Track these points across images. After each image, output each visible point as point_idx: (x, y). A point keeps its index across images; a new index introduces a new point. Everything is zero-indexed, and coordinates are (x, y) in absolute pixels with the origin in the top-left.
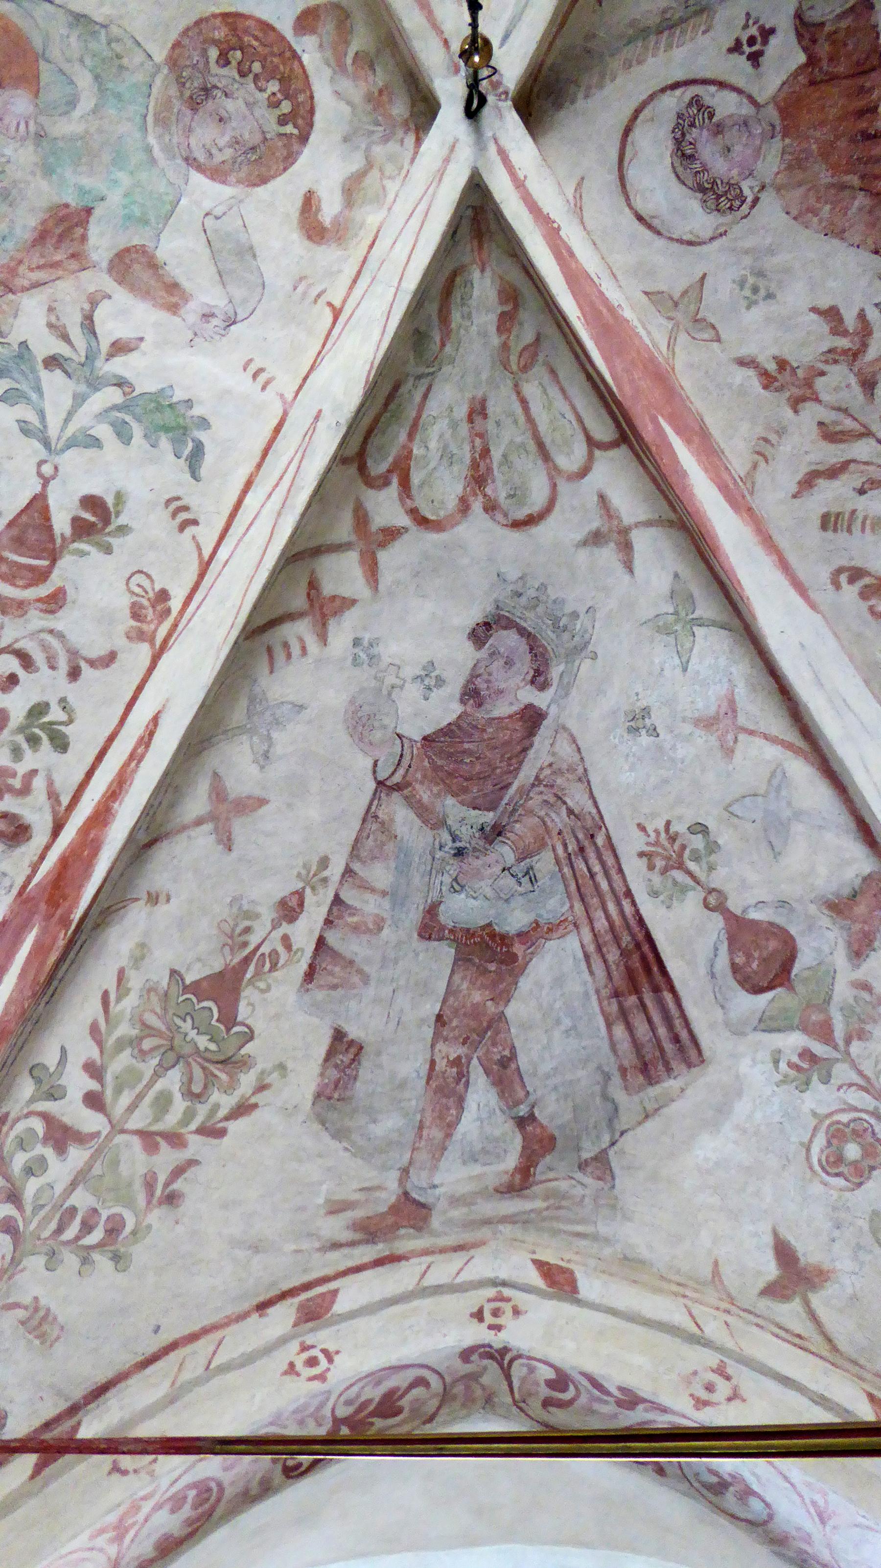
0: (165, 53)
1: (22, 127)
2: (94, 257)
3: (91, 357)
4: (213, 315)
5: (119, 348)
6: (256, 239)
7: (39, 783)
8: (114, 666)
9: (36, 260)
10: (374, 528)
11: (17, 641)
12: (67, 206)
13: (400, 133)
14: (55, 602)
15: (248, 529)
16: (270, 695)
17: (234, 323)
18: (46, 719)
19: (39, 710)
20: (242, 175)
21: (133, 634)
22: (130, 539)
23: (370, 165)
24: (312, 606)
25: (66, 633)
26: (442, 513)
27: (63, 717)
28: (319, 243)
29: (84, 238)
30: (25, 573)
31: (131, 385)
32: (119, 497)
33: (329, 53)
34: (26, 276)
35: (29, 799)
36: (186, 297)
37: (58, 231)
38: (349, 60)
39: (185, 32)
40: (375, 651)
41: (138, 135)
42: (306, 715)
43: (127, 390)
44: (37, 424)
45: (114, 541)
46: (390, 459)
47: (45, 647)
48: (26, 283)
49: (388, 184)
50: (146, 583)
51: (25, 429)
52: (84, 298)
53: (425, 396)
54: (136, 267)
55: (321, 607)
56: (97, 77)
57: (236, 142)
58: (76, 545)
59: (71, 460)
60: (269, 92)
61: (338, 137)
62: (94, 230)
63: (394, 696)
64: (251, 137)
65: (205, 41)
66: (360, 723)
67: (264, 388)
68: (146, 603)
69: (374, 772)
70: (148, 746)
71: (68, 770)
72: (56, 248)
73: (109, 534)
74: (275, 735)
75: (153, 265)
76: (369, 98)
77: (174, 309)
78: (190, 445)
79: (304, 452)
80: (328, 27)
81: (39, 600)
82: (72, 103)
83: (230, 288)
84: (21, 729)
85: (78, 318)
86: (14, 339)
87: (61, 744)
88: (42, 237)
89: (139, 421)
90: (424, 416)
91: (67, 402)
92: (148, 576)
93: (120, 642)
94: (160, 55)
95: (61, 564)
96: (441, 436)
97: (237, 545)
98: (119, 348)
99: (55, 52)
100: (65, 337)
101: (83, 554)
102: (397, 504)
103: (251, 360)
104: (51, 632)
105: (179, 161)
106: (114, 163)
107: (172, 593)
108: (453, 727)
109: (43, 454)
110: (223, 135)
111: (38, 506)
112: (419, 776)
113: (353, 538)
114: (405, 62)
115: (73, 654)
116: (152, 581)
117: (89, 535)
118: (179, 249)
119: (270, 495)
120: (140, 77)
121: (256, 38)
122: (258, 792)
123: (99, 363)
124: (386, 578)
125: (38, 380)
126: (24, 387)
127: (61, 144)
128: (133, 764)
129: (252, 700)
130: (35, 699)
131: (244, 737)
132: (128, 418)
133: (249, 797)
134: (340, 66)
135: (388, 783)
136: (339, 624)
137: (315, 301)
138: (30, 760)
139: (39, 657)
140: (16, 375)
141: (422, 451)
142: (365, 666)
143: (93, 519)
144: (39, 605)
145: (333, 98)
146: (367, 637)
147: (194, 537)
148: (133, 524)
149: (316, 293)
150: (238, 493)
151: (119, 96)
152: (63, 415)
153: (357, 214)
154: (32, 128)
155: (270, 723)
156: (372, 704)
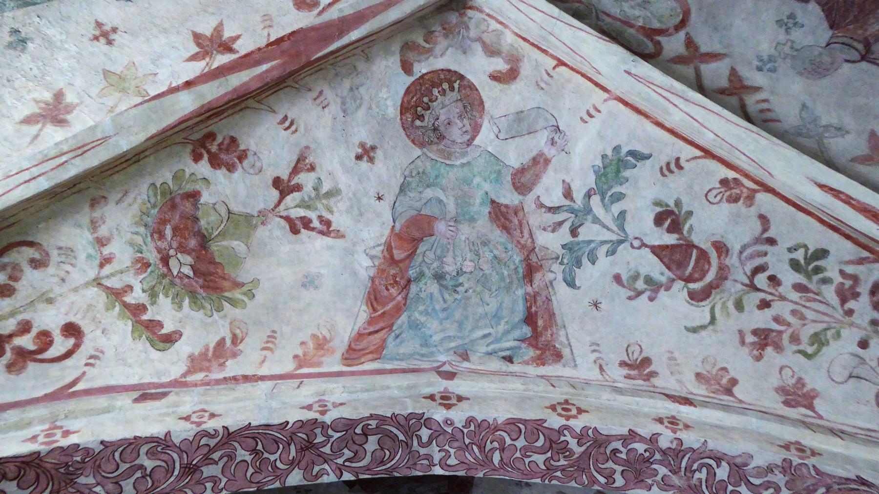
0: (417, 149)
1: (451, 228)
2: (516, 202)
3: (572, 211)
4: (553, 139)
5: (568, 194)
6: (513, 110)
7: (850, 269)
8: (769, 216)
9: (517, 233)
10: (686, 53)
11: (745, 273)
12: (490, 213)
13: (466, 19)
14: (721, 248)
15: (696, 120)
16: (795, 124)
17: (558, 127)
18: (802, 262)
19: (795, 265)
20: (478, 115)
21: (748, 203)
22: (685, 200)
23: (480, 39)
24: (735, 94)
25: (742, 244)
26: (679, 10)
27: (802, 250)
28: (518, 73)
29: (507, 206)
30: (700, 265)
31: (590, 190)
32: (657, 203)
33: (423, 57)
34: (526, 239)
35: (861, 277)
36: (541, 154)
37: (503, 219)
38: (427, 46)
39: (408, 136)
40: (766, 58)
41: (455, 169)
42: (809, 103)
43: (592, 192)
44: (609, 245)
45: (685, 209)
46: (645, 39)
47: (751, 257)
48: (530, 240)
49: (491, 28)
50: (715, 192)
51: (612, 252)
52: (539, 211)
53: (608, 15)
54: (522, 180)
55: (736, 88)
56: (428, 186)
57: (460, 117)
58: (685, 232)
59: (632, 229)
60: (438, 94)
61: (463, 57)
62: (503, 201)
63: (799, 48)
64: (457, 109)
65: (412, 126)
66: (816, 70)
67: (599, 111)
68: (728, 193)
69: (854, 62)
70: (840, 192)
71: (841, 249)
72: (511, 222)
73: (680, 212)
74: (824, 123)
75: (522, 170)
76: (446, 36)
77: (547, 161)
78: (629, 158)
79: (649, 83)
80: (411, 56)
81: (719, 257)
82: (440, 201)
83: (538, 128)
84: (809, 277)
85: (550, 215)
86: (560, 252)
87: (822, 253)
88: (506, 229)
89: (611, 187)
90: (619, 16)
91: (597, 227)
92: (710, 190)
93: (753, 211)
94: (417, 152)
95: (696, 243)
96: (632, 7)
97: (705, 127)
98: (568, 194)
99: (418, 205)
100: (561, 223)
101: (691, 228)
102: (672, 38)
103: (581, 118)
104: (741, 252)
105: (469, 149)
106: (469, 185)
107: (723, 177)
108: (826, 8)
110: (456, 124)
111: (658, 251)
112: (860, 32)
113: (692, 66)
114: (432, 12)
115: (757, 241)
116: (714, 188)
117: (679, 224)
118: (515, 155)
119: (675, 105)
120: (428, 164)
121: (413, 98)
122: (865, 136)
123: (576, 207)
124: (717, 48)
125: (583, 241)
126: (587, 250)
127: (459, 211)
128: (853, 202)
129: (800, 135)
130: (787, 267)
131: (826, 141)
132: (610, 194)
133: (869, 142)
134: (430, 51)
135: (863, 52)
136: (747, 79)
137: (551, 77)
138: (833, 273)
139: (758, 261)
140: (580, 253)
141: (641, 20)
142: (776, 65)
143: (669, 221)
144: (722, 258)
145: (444, 59)
146: (756, 63)
147: (687, 161)
148: (675, 197)
149: (547, 76)
150: (662, 131)
151: (437, 177)
152: (605, 230)
153: (505, 48)
154: (452, 224)
155: (816, 125)
156: (803, 63)
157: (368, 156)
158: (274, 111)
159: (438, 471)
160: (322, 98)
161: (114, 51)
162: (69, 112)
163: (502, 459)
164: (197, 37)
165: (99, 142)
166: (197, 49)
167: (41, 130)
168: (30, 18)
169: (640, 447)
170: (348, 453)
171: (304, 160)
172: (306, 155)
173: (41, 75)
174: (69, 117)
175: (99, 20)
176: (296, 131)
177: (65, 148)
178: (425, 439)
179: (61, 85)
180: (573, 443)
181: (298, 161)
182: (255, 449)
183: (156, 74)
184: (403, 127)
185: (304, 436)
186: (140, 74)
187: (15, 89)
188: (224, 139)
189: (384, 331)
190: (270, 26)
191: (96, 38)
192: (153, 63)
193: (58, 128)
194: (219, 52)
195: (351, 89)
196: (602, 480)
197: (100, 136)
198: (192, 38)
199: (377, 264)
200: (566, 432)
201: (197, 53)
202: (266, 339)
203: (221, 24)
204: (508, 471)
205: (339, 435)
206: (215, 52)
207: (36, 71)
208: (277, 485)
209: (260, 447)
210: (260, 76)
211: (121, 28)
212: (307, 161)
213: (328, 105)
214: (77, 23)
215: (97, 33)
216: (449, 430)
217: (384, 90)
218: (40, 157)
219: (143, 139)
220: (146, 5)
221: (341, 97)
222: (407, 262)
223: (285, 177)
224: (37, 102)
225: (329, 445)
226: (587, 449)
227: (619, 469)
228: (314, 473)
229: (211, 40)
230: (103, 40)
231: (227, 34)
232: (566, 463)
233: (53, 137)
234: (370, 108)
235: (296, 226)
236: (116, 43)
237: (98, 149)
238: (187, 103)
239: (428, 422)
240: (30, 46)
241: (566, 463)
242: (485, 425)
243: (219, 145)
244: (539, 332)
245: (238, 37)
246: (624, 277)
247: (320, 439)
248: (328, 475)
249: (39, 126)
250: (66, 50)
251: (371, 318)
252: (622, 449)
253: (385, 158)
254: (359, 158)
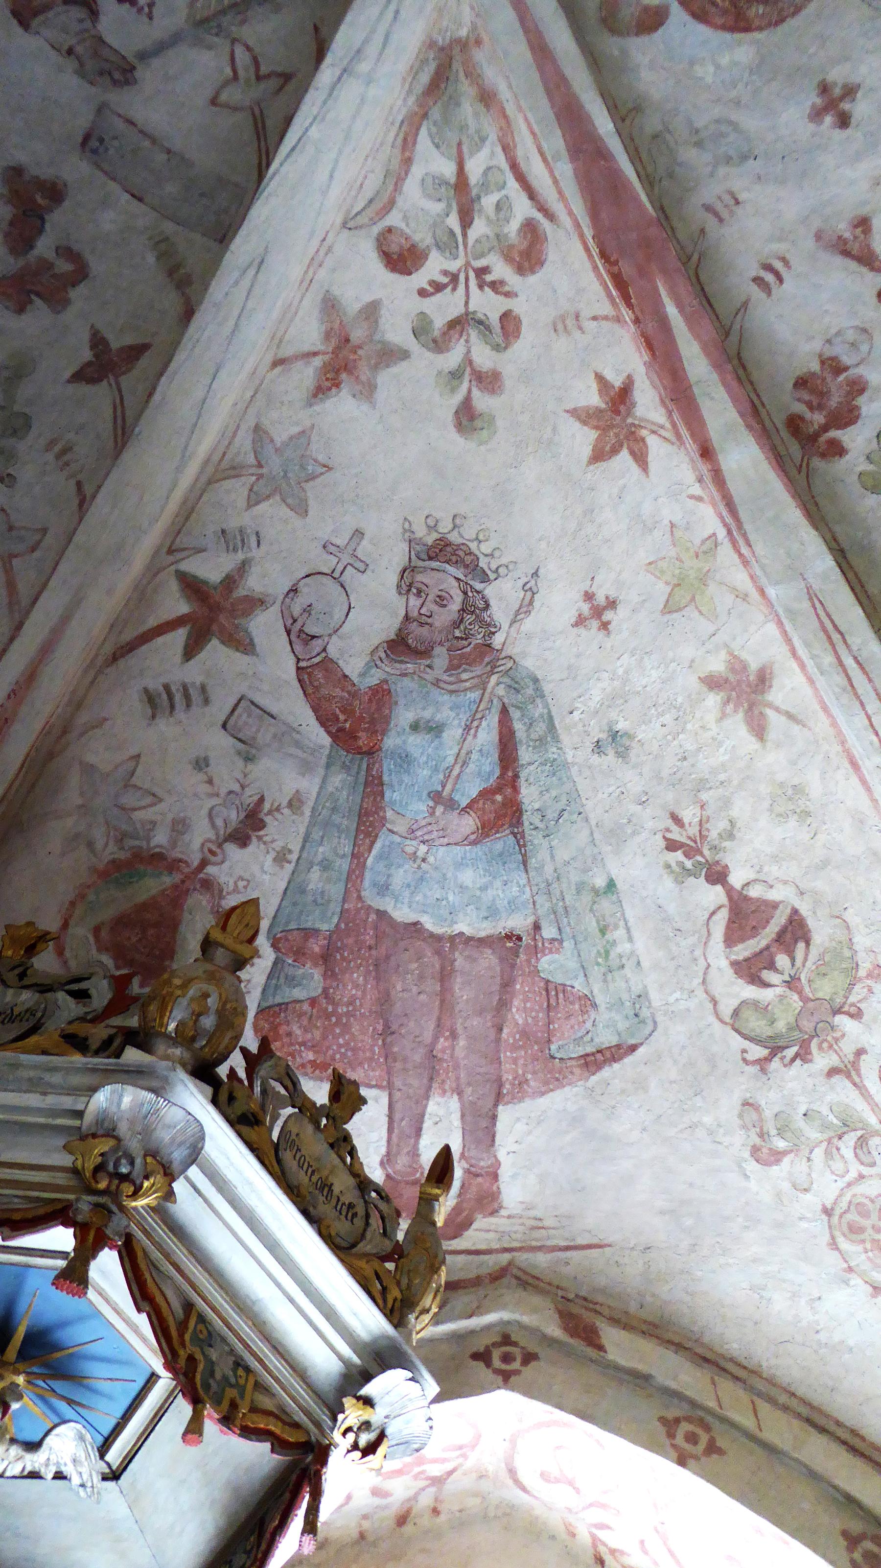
157: (842, 98)
158: (745, 305)
160: (719, 207)
161: (629, 597)
162: (745, 667)
164: (599, 455)
165: (818, 605)
166: (625, 454)
167: (777, 710)
168: (575, 725)
171: (845, 242)
172: (835, 238)
173: (674, 711)
174: (754, 666)
175: (573, 620)
176: (784, 260)
177: (829, 659)
179: (692, 681)
181: (846, 253)
183: (672, 525)
184: (777, 24)
186: (673, 553)
187: (699, 749)
188: (799, 400)
190: (577, 317)
191: (605, 626)
192: (650, 531)
193: (775, 683)
194: (629, 413)
195: (699, 144)
197: (806, 604)
198: (602, 465)
201: (632, 453)
203: (574, 413)
206: (630, 420)
207: (668, 718)
210: (690, 321)
211: (585, 586)
212: (847, 235)
213: (732, 194)
214: (578, 656)
215: (595, 624)
217: (699, 71)
218: (846, 698)
219: (813, 532)
220: (543, 545)
221: (715, 166)
224: (723, 716)
229: (604, 430)
230: (608, 616)
231: (594, 399)
233: (790, 687)
234: (737, 103)
236: (613, 594)
237: (831, 609)
238: (745, 458)
240: (621, 725)
243: (811, 408)
245: (600, 378)
249: (769, 712)
250: (626, 672)
253: (847, 59)
254: (844, 121)
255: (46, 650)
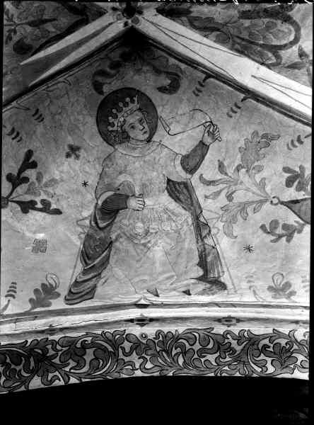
17: (211, 122)
32: (286, 170)
67: (239, 108)
100: (219, 193)
109: (268, 203)
159: (139, 373)
163: (185, 361)
169: (283, 342)
170: (72, 364)
178: (127, 350)
180: (234, 343)
182: (5, 362)
185: (40, 351)
189: (94, 279)
196: (259, 370)
199: (86, 231)
200: (228, 336)
202: (11, 285)
204: (191, 370)
205: (64, 349)
208: (23, 388)
209: (8, 361)
216: (144, 341)
222: (108, 229)
223: (15, 173)
225: (58, 357)
226: (244, 347)
227: (269, 360)
228: (49, 379)
232: (230, 359)
235: (27, 207)
239: (128, 337)
241: (230, 359)
242: (170, 335)
244: (210, 278)
246: (268, 226)
247: (51, 352)
248: (60, 380)
251: (84, 270)
252: (270, 344)
255: (104, 29)
